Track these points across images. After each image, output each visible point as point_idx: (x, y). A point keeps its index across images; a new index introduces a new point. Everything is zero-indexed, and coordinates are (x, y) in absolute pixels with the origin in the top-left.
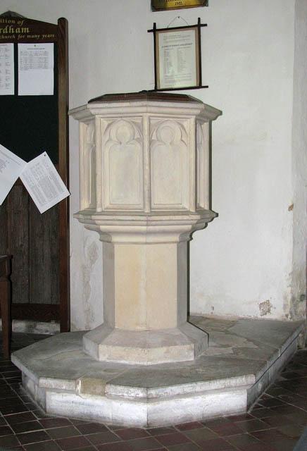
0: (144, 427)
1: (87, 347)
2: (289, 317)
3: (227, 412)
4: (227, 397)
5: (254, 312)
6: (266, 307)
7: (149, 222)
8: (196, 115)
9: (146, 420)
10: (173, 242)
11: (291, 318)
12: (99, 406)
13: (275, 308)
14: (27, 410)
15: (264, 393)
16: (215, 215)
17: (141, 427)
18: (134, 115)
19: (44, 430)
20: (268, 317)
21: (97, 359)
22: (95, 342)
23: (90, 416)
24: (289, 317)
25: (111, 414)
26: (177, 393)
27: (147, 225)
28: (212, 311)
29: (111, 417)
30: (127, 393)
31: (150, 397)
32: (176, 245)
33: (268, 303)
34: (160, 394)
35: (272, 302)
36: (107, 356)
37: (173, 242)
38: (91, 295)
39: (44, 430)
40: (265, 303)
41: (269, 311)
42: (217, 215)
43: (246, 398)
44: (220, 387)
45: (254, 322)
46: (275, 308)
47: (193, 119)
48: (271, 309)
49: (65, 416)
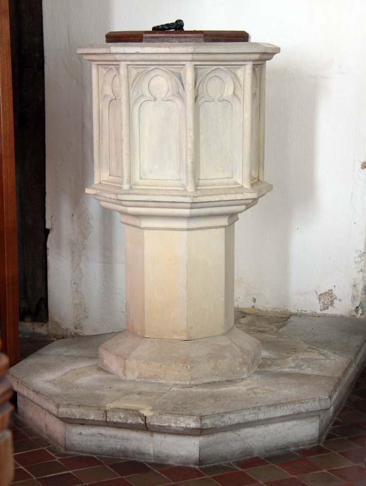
0: (195, 464)
1: (106, 362)
2: (360, 311)
3: (296, 445)
4: (296, 425)
5: (313, 306)
6: (328, 298)
7: (194, 205)
8: (253, 61)
9: (198, 456)
10: (221, 227)
11: (362, 314)
12: (137, 440)
13: (340, 300)
14: (40, 447)
15: (335, 418)
16: (212, 100)
17: (192, 466)
18: (174, 63)
19: (70, 472)
20: (330, 311)
21: (124, 378)
22: (118, 356)
23: (124, 452)
24: (360, 311)
25: (152, 449)
26: (236, 422)
27: (191, 208)
28: (253, 304)
29: (151, 452)
30: (175, 423)
31: (204, 427)
32: (223, 230)
33: (330, 293)
34: (216, 423)
35: (336, 292)
36: (137, 374)
37: (221, 227)
38: (342, 456)
39: (70, 472)
40: (326, 293)
41: (332, 303)
42: (271, 186)
43: (318, 425)
44: (288, 413)
45: (314, 316)
46: (340, 300)
47: (249, 66)
48: (335, 301)
49: (91, 453)
